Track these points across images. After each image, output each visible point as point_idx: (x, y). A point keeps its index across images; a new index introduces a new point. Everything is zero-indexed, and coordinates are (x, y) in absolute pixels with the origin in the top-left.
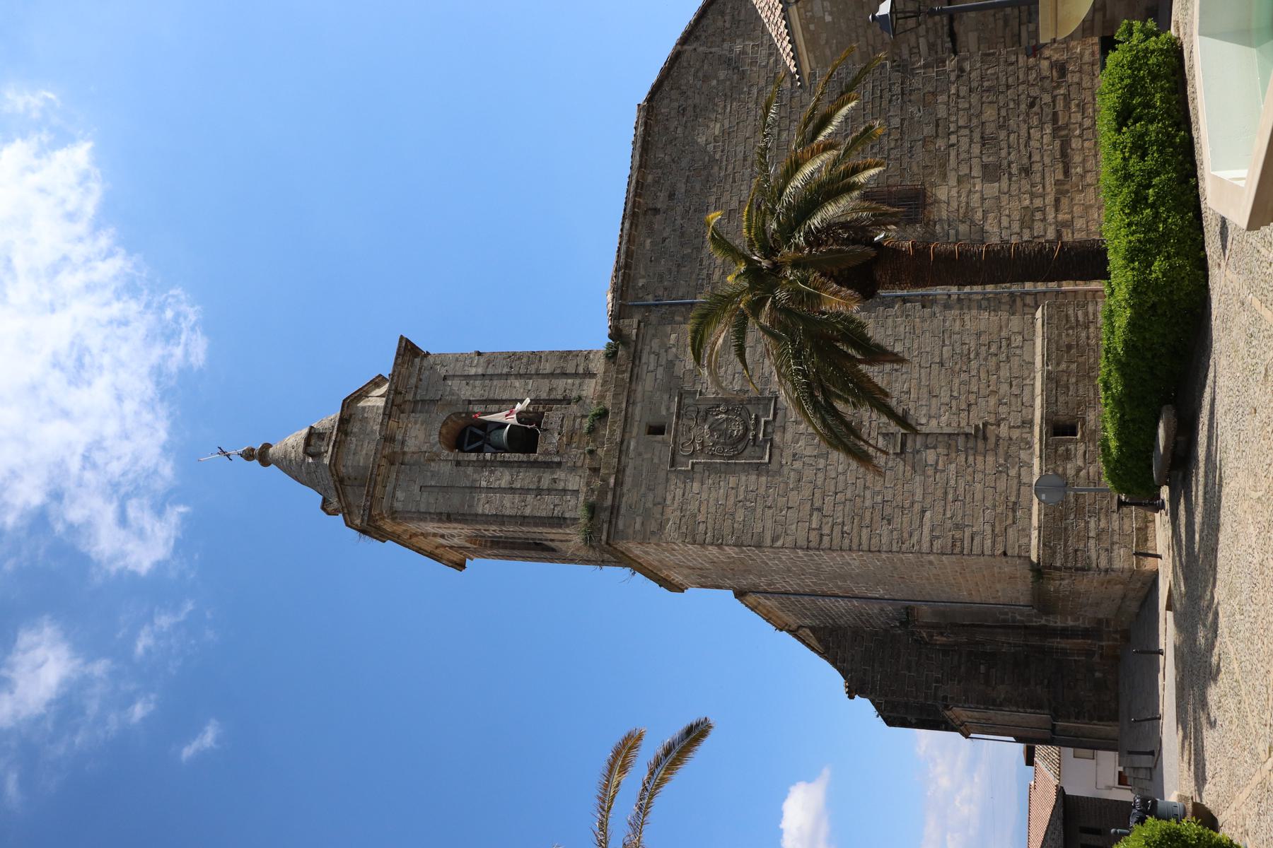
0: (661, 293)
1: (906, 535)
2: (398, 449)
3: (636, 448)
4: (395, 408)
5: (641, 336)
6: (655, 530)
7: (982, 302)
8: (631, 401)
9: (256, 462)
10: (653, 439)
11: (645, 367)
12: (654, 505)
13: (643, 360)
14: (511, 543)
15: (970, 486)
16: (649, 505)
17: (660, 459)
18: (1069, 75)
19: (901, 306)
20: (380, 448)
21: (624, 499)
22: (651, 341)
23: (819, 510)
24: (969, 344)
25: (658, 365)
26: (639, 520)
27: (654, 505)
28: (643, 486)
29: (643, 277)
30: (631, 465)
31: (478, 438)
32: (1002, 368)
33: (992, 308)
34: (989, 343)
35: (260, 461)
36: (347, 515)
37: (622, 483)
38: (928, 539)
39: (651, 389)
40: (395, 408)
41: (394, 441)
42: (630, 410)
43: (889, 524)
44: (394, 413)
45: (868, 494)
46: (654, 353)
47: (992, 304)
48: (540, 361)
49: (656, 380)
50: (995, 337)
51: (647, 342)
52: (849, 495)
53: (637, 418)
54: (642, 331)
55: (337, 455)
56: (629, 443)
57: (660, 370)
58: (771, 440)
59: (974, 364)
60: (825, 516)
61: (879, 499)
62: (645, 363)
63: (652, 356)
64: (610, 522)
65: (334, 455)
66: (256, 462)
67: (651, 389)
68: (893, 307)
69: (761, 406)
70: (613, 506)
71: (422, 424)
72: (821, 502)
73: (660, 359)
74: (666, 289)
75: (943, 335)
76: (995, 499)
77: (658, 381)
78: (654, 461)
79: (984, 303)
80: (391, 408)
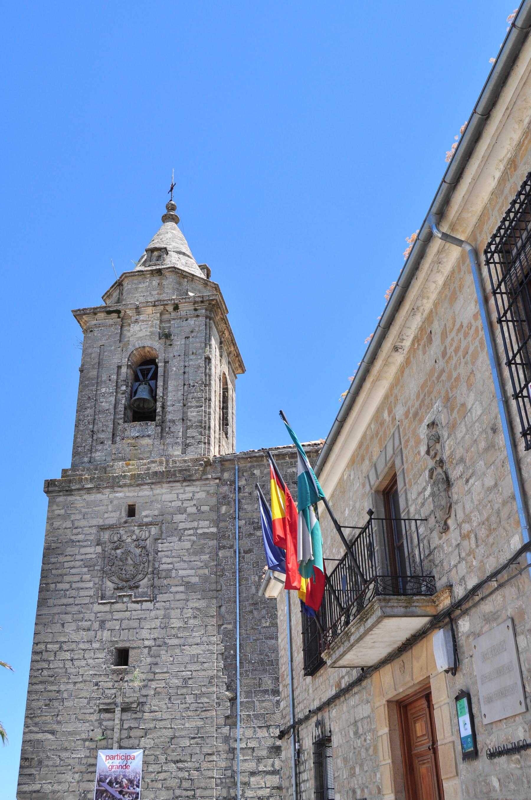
0: (247, 490)
1: (37, 720)
2: (133, 319)
3: (117, 498)
4: (162, 307)
5: (207, 482)
6: (54, 526)
7: (230, 771)
8: (153, 486)
9: (165, 212)
10: (123, 510)
11: (182, 491)
12: (72, 521)
13: (187, 489)
14: (223, 420)
15: (71, 770)
16: (73, 517)
17: (107, 518)
18: (302, 785)
19: (227, 697)
20: (130, 306)
21: (78, 498)
22: (204, 491)
23: (61, 648)
24: (191, 761)
25: (183, 501)
26: (62, 512)
27: (72, 521)
28: (86, 510)
29: (261, 473)
30: (103, 497)
31: (145, 375)
32: (167, 792)
33: (224, 781)
34: (191, 779)
35: (166, 215)
36: (106, 296)
37: (89, 493)
38: (32, 738)
39: (163, 500)
40: (162, 307)
41: (139, 315)
42: (146, 487)
43: (46, 705)
44: (158, 308)
45: (71, 686)
46: (194, 495)
47: (227, 781)
48: (197, 407)
49: (171, 502)
50: (197, 784)
51: (203, 488)
52: (69, 671)
53: (140, 494)
54: (212, 483)
55: (133, 276)
56: (120, 492)
57: (179, 504)
58: (116, 602)
59: (172, 767)
60: (55, 653)
61: (65, 695)
62: (185, 491)
63: (191, 495)
64: (60, 491)
65: (132, 274)
66: (165, 212)
67: (163, 500)
68: (228, 690)
69: (146, 590)
70: (72, 490)
71: (151, 332)
72: (66, 649)
73: (188, 502)
74: (250, 494)
75: (199, 737)
76: (59, 792)
77: (170, 504)
78: (106, 514)
79: (229, 773)
80: (162, 305)
